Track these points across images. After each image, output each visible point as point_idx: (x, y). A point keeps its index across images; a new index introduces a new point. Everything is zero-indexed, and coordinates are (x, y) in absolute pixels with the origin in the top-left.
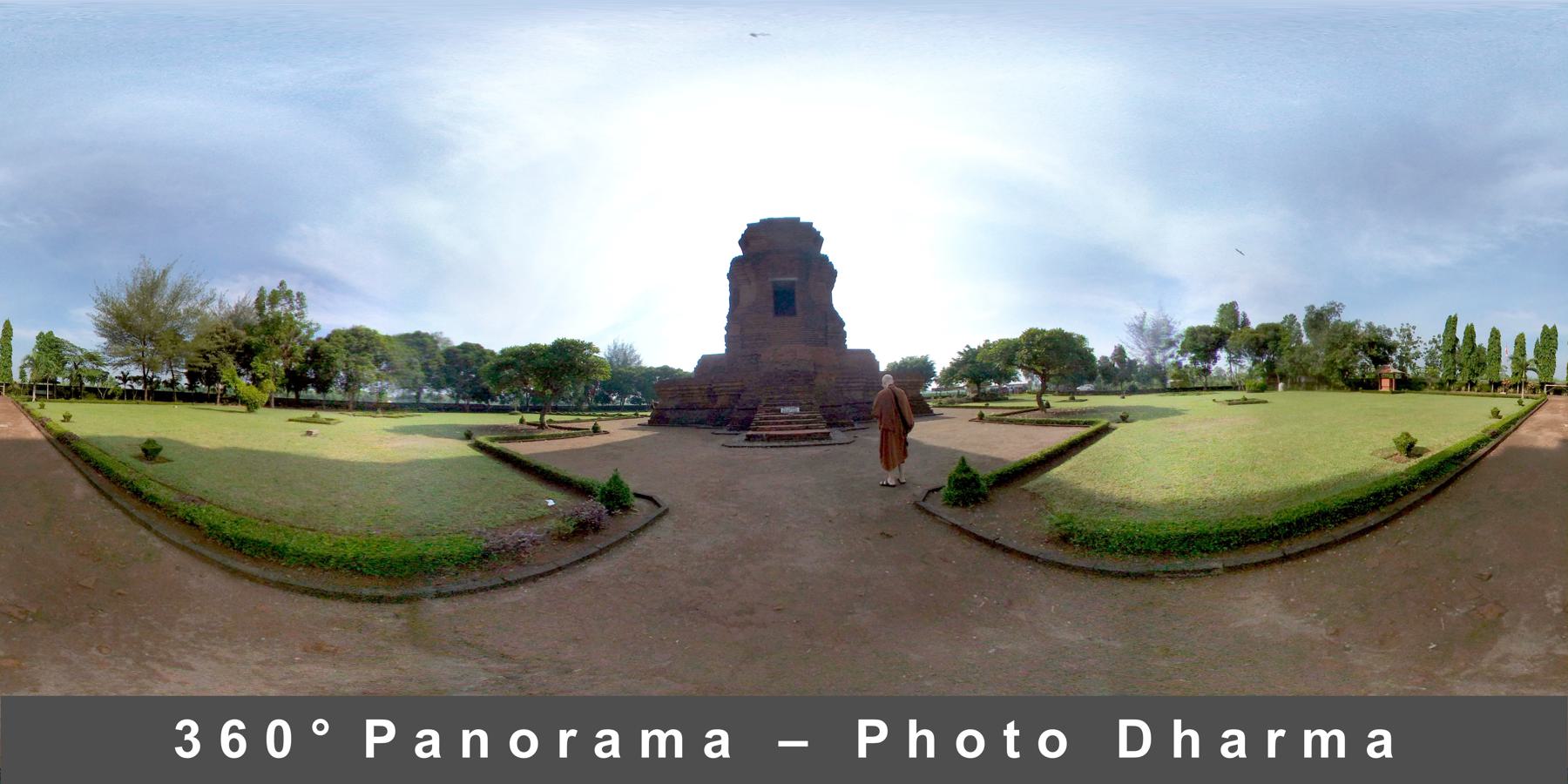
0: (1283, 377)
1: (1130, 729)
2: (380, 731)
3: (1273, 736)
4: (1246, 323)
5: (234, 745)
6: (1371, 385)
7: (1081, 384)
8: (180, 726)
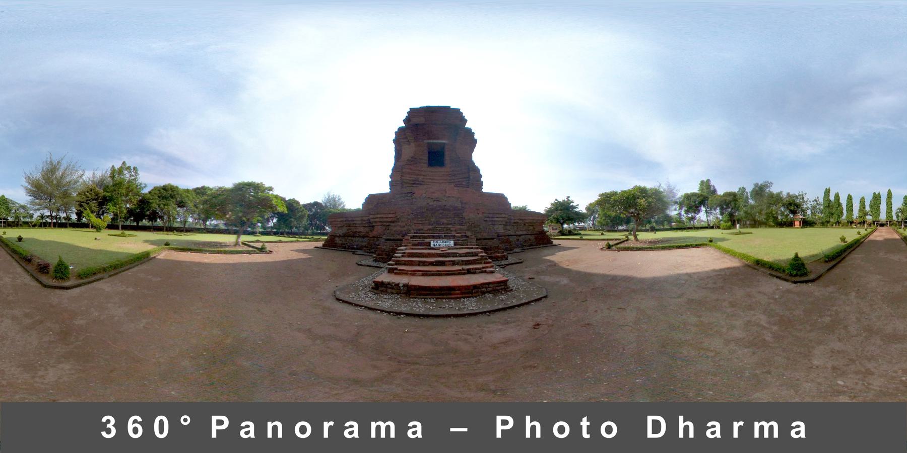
0: (739, 221)
1: (653, 421)
2: (220, 423)
3: (736, 425)
4: (714, 191)
5: (135, 431)
6: (790, 224)
7: (621, 225)
8: (104, 420)
